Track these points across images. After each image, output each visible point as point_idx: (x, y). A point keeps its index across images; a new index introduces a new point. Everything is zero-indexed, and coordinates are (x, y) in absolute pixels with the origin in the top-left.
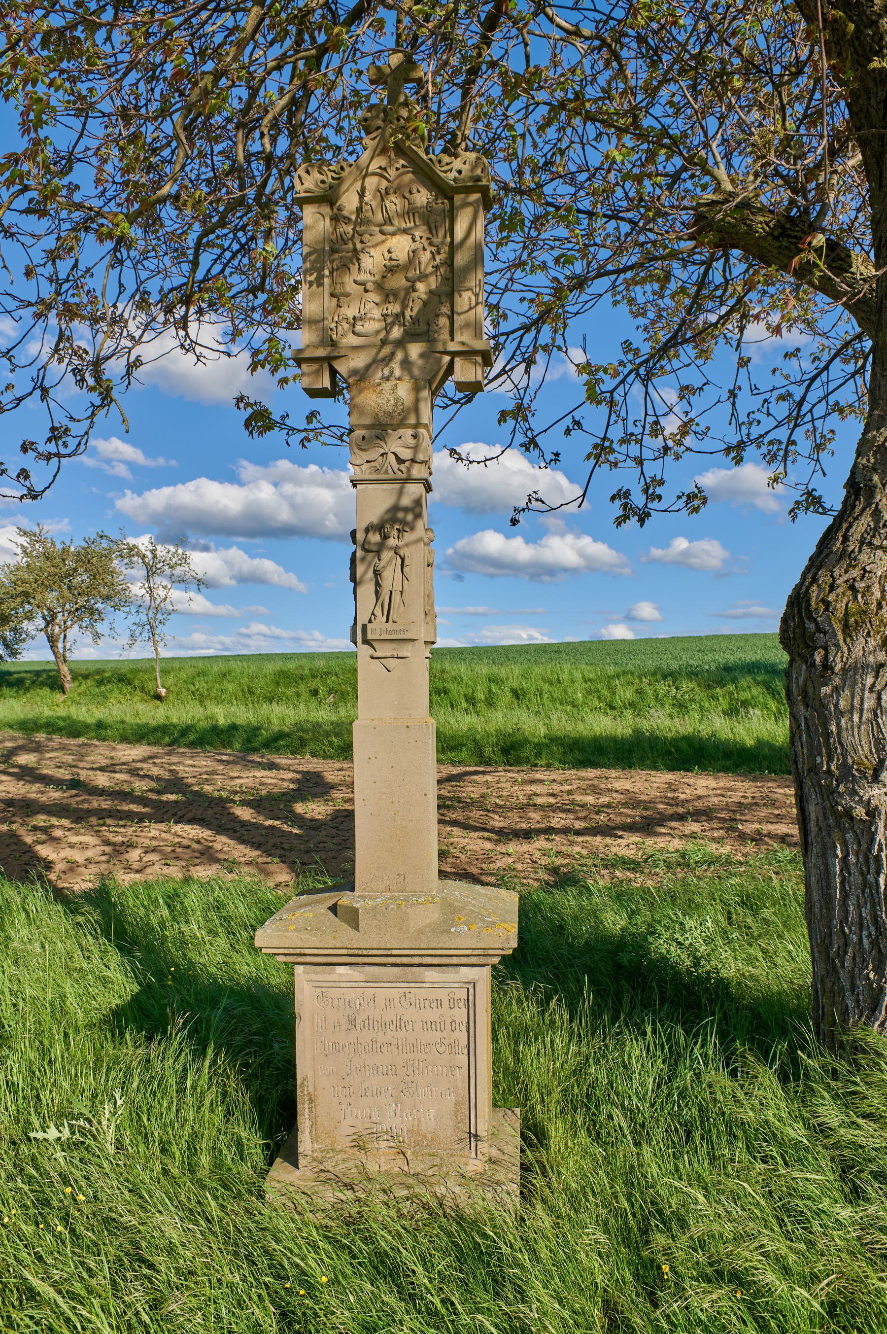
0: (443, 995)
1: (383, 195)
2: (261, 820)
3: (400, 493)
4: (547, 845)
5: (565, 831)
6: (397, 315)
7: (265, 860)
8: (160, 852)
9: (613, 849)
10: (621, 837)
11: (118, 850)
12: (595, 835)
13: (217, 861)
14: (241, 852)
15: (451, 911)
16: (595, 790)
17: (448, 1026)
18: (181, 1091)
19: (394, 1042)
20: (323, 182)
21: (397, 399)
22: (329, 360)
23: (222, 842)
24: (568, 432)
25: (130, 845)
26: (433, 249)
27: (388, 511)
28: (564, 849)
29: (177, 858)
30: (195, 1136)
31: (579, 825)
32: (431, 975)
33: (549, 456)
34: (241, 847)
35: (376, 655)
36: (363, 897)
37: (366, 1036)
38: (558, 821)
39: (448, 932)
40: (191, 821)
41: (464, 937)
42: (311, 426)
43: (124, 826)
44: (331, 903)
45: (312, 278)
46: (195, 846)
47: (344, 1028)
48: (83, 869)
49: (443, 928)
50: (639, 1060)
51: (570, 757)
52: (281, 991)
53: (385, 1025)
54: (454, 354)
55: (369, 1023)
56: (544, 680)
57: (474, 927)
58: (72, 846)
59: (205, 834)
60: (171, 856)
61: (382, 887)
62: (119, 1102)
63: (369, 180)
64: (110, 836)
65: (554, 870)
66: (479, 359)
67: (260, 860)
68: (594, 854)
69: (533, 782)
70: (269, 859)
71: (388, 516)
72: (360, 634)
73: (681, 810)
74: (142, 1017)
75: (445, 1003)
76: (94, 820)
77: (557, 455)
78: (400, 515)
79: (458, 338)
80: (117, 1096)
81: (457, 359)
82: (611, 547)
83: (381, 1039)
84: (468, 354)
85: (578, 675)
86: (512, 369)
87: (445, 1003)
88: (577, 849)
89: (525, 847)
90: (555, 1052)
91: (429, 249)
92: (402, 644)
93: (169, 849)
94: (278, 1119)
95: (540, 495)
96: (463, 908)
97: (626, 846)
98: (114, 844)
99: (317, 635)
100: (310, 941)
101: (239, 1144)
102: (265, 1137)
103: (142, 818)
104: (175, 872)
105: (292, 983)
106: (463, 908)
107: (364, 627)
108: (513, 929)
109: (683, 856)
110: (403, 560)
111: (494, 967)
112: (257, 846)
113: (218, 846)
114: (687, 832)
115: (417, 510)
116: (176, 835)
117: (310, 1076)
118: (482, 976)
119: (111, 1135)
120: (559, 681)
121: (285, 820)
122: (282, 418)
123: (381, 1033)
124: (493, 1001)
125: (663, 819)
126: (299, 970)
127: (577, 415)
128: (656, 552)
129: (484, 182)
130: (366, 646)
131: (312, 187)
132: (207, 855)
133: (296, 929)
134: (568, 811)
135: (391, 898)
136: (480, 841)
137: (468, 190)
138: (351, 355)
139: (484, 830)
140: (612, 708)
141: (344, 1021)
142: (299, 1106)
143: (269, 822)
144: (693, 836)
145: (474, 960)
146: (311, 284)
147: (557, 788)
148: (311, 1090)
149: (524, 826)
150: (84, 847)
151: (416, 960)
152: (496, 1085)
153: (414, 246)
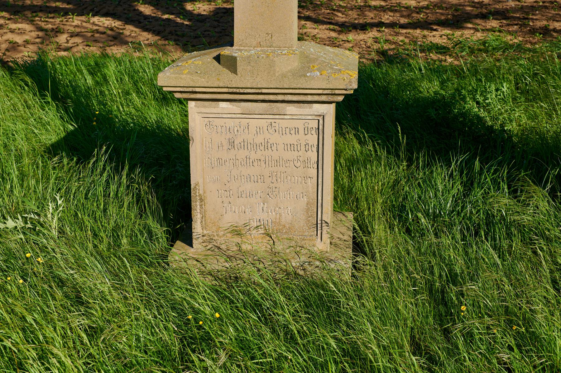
0: (299, 124)
2: (159, 14)
4: (378, 35)
5: (392, 25)
7: (163, 42)
8: (82, 36)
9: (430, 39)
10: (436, 30)
11: (48, 35)
12: (415, 28)
13: (126, 43)
14: (145, 37)
15: (308, 62)
17: (303, 148)
18: (106, 195)
19: (263, 158)
23: (130, 30)
25: (57, 31)
28: (391, 38)
29: (96, 41)
30: (117, 228)
31: (403, 21)
32: (291, 109)
34: (145, 34)
36: (241, 50)
37: (242, 154)
38: (387, 18)
39: (305, 76)
40: (106, 15)
41: (317, 81)
43: (53, 18)
44: (215, 54)
46: (109, 32)
47: (226, 148)
48: (22, 48)
49: (302, 73)
50: (443, 185)
52: (178, 134)
53: (256, 146)
55: (244, 145)
57: (325, 73)
58: (12, 31)
59: (117, 24)
60: (92, 38)
61: (254, 43)
62: (60, 202)
64: (43, 24)
65: (382, 53)
67: (160, 42)
68: (414, 41)
70: (167, 42)
73: (484, 11)
74: (76, 147)
75: (301, 131)
76: (29, 14)
80: (58, 198)
83: (253, 156)
87: (301, 131)
88: (401, 38)
89: (362, 36)
90: (381, 175)
93: (89, 34)
94: (179, 219)
96: (317, 59)
97: (439, 36)
98: (46, 30)
100: (199, 82)
101: (150, 233)
102: (168, 226)
103: (66, 13)
104: (95, 50)
105: (187, 130)
106: (317, 59)
108: (355, 75)
109: (484, 43)
111: (338, 104)
112: (156, 33)
113: (127, 33)
114: (488, 27)
116: (94, 24)
117: (201, 181)
118: (330, 110)
119: (55, 223)
121: (178, 15)
123: (253, 152)
124: (336, 144)
125: (469, 18)
126: (191, 104)
132: (117, 38)
133: (189, 73)
134: (396, 11)
135: (262, 51)
136: (327, 32)
139: (330, 23)
141: (225, 143)
142: (193, 204)
143: (166, 16)
144: (493, 30)
145: (324, 98)
148: (201, 192)
149: (361, 21)
150: (21, 32)
151: (280, 98)
152: (335, 199)
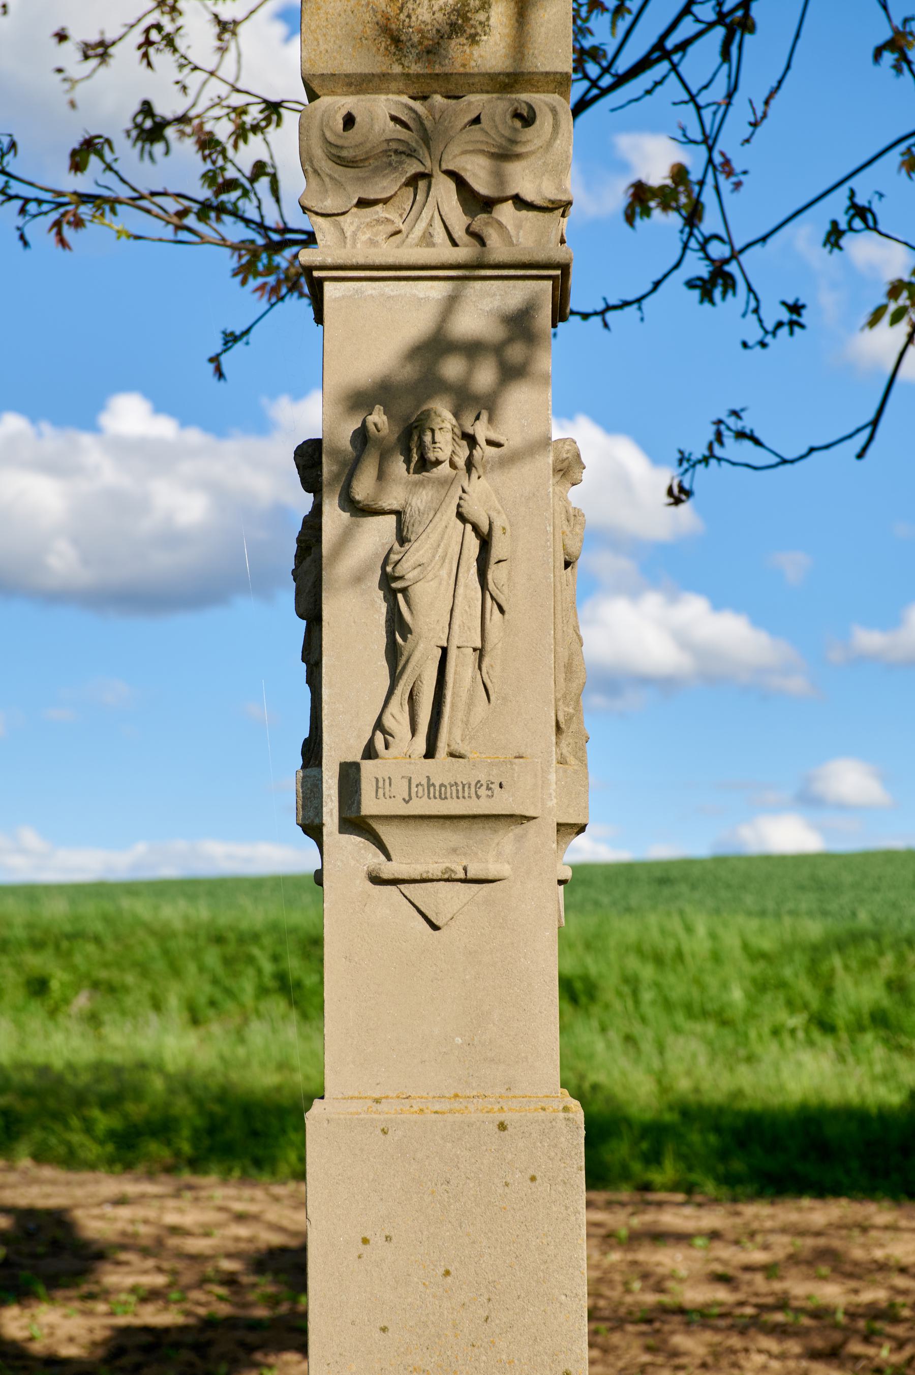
3: (451, 303)
16: (828, 1260)
24: (834, 237)
33: (774, 313)
35: (389, 870)
51: (738, 1166)
56: (640, 952)
69: (659, 1237)
72: (332, 796)
77: (796, 308)
82: (757, 621)
85: (731, 941)
86: (683, 47)
92: (481, 833)
95: (747, 423)
99: (30, 838)
107: (350, 775)
110: (485, 543)
120: (679, 955)
127: (864, 190)
128: (869, 639)
130: (355, 841)
140: (827, 1027)
147: (730, 1256)
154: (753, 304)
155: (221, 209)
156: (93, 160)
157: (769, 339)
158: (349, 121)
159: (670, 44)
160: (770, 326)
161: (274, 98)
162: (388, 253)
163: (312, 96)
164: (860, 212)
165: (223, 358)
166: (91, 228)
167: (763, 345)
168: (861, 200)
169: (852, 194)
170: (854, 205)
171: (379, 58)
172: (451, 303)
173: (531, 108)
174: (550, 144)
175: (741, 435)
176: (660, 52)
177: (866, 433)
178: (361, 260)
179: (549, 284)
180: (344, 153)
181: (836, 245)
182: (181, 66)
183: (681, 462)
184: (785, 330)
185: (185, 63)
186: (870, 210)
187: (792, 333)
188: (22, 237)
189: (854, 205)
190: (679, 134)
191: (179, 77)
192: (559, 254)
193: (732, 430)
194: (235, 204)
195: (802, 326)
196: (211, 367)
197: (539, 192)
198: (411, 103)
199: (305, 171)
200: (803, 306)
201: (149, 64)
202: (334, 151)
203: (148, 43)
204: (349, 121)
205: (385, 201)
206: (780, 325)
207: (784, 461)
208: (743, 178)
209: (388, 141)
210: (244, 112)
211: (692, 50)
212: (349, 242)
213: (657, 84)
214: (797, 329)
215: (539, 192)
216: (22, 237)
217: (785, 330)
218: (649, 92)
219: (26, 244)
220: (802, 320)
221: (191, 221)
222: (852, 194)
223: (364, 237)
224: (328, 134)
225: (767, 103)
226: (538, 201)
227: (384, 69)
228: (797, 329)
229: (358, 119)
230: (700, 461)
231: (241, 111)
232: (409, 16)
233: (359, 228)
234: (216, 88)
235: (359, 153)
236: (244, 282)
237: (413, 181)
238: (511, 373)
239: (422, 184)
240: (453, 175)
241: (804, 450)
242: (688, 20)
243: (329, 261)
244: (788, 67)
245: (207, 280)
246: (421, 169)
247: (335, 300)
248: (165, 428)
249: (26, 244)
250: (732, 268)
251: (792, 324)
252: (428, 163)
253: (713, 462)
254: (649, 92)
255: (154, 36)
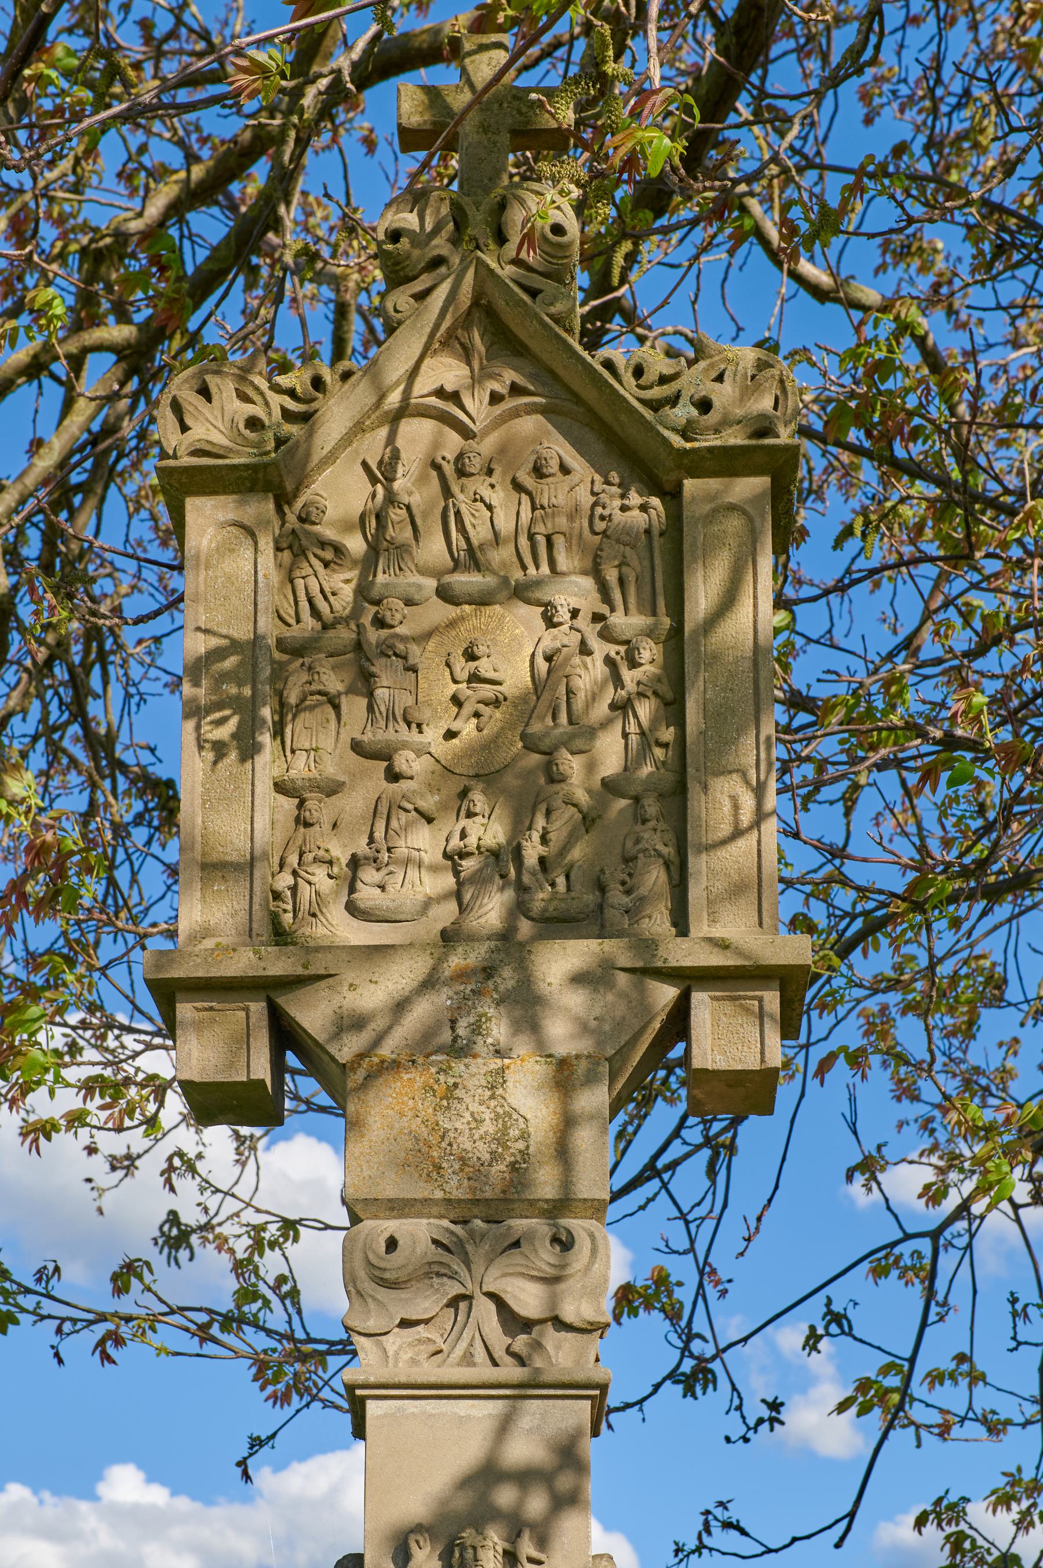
1: (448, 475)
3: (504, 1426)
6: (495, 854)
20: (253, 423)
21: (505, 1117)
22: (268, 989)
26: (612, 649)
27: (466, 1482)
33: (756, 1410)
42: (125, 1305)
45: (223, 733)
54: (690, 979)
63: (410, 421)
66: (772, 999)
71: (462, 1502)
78: (505, 1496)
79: (700, 927)
81: (700, 999)
84: (735, 978)
91: (600, 648)
95: (734, 1514)
115: (564, 1482)
122: (40, 1275)
127: (840, 1295)
129: (785, 436)
131: (219, 439)
137: (727, 463)
138: (349, 976)
146: (220, 749)
153: (550, 640)
154: (736, 1402)
155: (242, 1320)
156: (134, 1282)
157: (750, 1434)
158: (392, 1244)
159: (660, 1164)
160: (752, 1423)
161: (292, 1216)
162: (430, 1371)
163: (355, 1219)
164: (835, 1318)
165: (249, 1462)
166: (133, 1347)
167: (746, 1440)
168: (836, 1308)
169: (829, 1302)
170: (830, 1312)
171: (422, 1184)
172: (504, 1426)
173: (569, 1233)
174: (588, 1268)
175: (727, 1525)
176: (650, 1171)
177: (844, 1524)
178: (403, 1379)
179: (588, 1404)
180: (387, 1275)
181: (814, 1348)
182: (202, 1190)
183: (677, 1552)
184: (766, 1426)
185: (206, 1186)
186: (845, 1316)
187: (772, 1429)
188: (57, 1355)
189: (830, 1312)
190: (662, 1246)
191: (202, 1199)
192: (598, 1374)
193: (720, 1520)
194: (255, 1315)
195: (782, 1423)
196: (239, 1471)
197: (578, 1314)
198: (452, 1227)
199: (348, 1292)
200: (782, 1404)
201: (172, 1189)
202: (377, 1273)
203: (171, 1168)
204: (392, 1244)
205: (427, 1321)
206: (760, 1421)
207: (770, 1551)
208: (727, 1286)
209: (430, 1264)
210: (264, 1230)
211: (679, 1169)
212: (391, 1361)
213: (650, 1200)
214: (776, 1425)
215: (578, 1314)
216: (57, 1355)
217: (766, 1426)
218: (642, 1208)
219: (60, 1361)
220: (782, 1417)
221: (215, 1330)
222: (829, 1302)
223: (406, 1356)
224: (371, 1257)
225: (759, 1219)
226: (578, 1323)
227: (426, 1194)
228: (776, 1425)
229: (401, 1243)
230: (693, 1552)
231: (260, 1228)
232: (450, 1145)
233: (401, 1347)
234: (231, 1206)
235: (402, 1275)
236: (263, 1388)
237: (454, 1303)
238: (567, 1501)
239: (463, 1305)
240: (492, 1296)
241: (787, 1541)
242: (677, 1142)
243: (372, 1379)
244: (777, 1187)
245: (228, 1389)
246: (462, 1290)
247: (377, 1418)
248: (157, 1495)
249: (60, 1361)
250: (716, 1366)
251: (772, 1421)
252: (469, 1285)
253: (705, 1552)
254: (642, 1208)
255: (177, 1162)
